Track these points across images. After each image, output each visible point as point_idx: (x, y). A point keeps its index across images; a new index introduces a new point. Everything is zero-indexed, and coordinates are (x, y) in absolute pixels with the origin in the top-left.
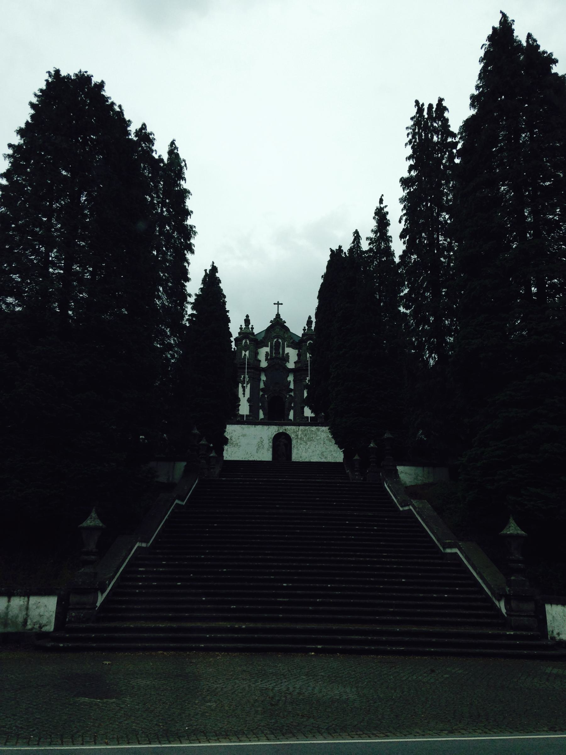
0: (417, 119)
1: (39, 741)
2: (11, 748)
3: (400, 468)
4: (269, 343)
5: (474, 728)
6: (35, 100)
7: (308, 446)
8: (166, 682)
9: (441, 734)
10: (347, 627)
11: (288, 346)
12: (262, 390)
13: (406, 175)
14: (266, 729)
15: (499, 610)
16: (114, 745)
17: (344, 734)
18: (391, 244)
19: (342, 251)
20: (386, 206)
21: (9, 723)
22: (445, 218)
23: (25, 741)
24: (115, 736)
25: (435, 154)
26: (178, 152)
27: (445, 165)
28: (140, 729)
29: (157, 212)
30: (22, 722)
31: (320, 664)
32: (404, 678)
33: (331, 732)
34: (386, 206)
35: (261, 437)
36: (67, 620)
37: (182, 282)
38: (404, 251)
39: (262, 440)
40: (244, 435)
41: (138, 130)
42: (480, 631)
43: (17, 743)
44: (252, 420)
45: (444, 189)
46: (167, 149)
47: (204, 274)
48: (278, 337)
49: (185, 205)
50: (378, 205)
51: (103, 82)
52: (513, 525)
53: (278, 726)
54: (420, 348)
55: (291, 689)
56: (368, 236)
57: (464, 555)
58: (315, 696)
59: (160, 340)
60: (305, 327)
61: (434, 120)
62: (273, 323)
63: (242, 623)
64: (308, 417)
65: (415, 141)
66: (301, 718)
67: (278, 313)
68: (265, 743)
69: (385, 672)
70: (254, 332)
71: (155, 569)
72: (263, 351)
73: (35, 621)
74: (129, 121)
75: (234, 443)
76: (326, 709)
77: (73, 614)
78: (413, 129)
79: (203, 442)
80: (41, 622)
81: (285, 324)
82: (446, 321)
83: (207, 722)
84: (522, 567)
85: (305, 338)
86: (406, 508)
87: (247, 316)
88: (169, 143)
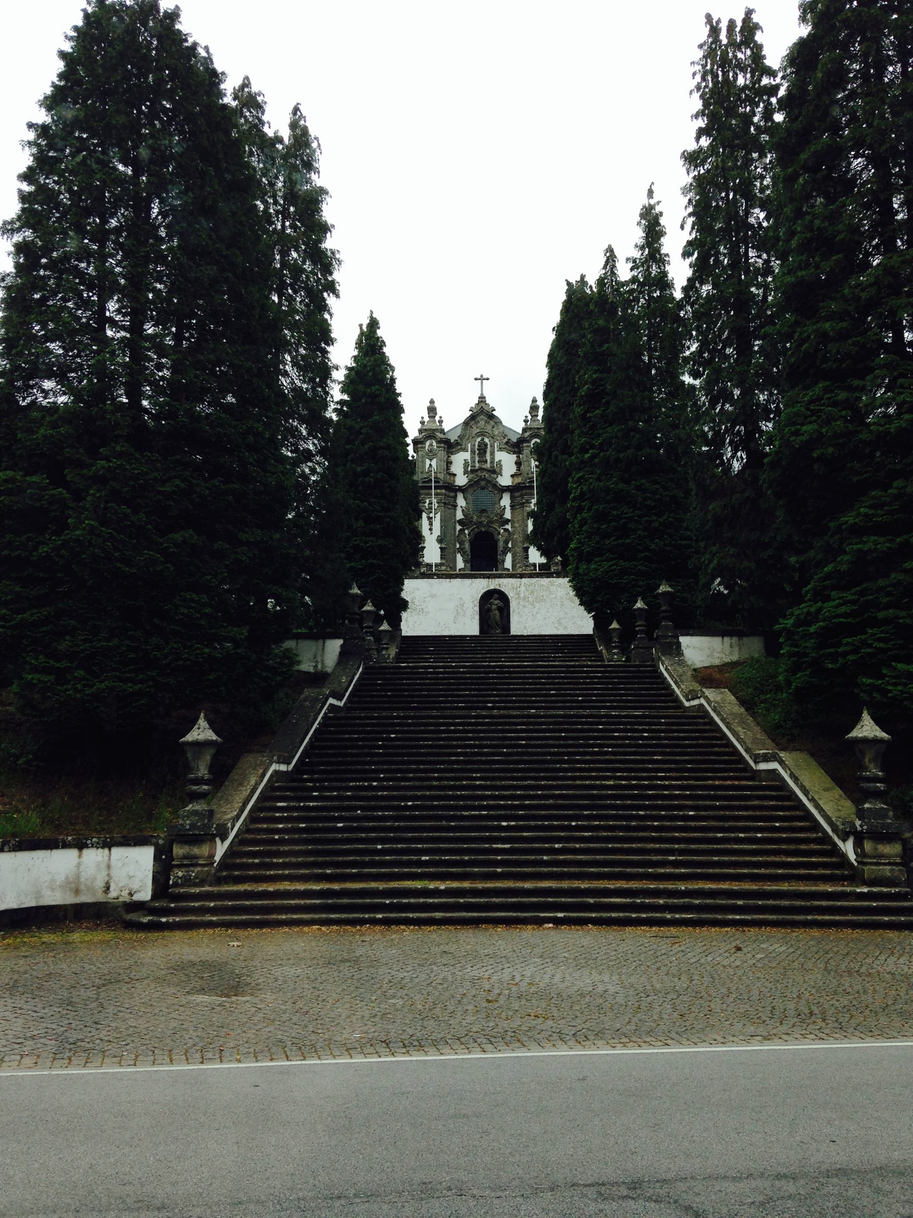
0: (710, 47)
1: (136, 1059)
2: (93, 1071)
3: (684, 640)
4: (469, 445)
5: (803, 1032)
6: (67, 47)
7: (535, 611)
8: (326, 971)
9: (753, 1041)
10: (602, 886)
11: (500, 449)
12: (460, 522)
13: (692, 146)
14: (480, 1036)
15: (844, 856)
16: (249, 1062)
17: (600, 1043)
18: (667, 268)
19: (586, 283)
20: (658, 203)
21: (90, 1035)
22: (759, 218)
23: (115, 1059)
24: (252, 1050)
25: (741, 106)
26: (307, 124)
27: (758, 128)
28: (289, 1039)
29: (275, 229)
30: (109, 1033)
31: (562, 940)
32: (693, 960)
33: (581, 1040)
34: (658, 203)
35: (461, 599)
36: (171, 882)
37: (323, 345)
38: (689, 280)
39: (462, 602)
40: (433, 596)
41: (237, 88)
42: (814, 888)
43: (102, 1063)
44: (445, 572)
45: (756, 168)
46: (287, 120)
47: (358, 332)
48: (482, 434)
49: (322, 216)
50: (645, 201)
51: (177, 7)
52: (867, 723)
53: (498, 1032)
54: (717, 442)
55: (518, 978)
56: (629, 256)
57: (789, 772)
58: (555, 987)
59: (292, 445)
60: (526, 417)
61: (738, 47)
62: (475, 411)
63: (439, 882)
64: (534, 565)
65: (706, 87)
66: (534, 1020)
67: (482, 394)
68: (479, 1056)
69: (663, 951)
70: (443, 427)
71: (302, 804)
72: (460, 460)
73: (121, 885)
74: (223, 73)
75: (418, 608)
76: (572, 1007)
77: (180, 874)
78: (702, 65)
79: (369, 607)
80: (131, 886)
81: (494, 412)
82: (761, 396)
83: (390, 1027)
84: (882, 789)
85: (526, 435)
86: (695, 702)
87: (432, 402)
88: (290, 110)
